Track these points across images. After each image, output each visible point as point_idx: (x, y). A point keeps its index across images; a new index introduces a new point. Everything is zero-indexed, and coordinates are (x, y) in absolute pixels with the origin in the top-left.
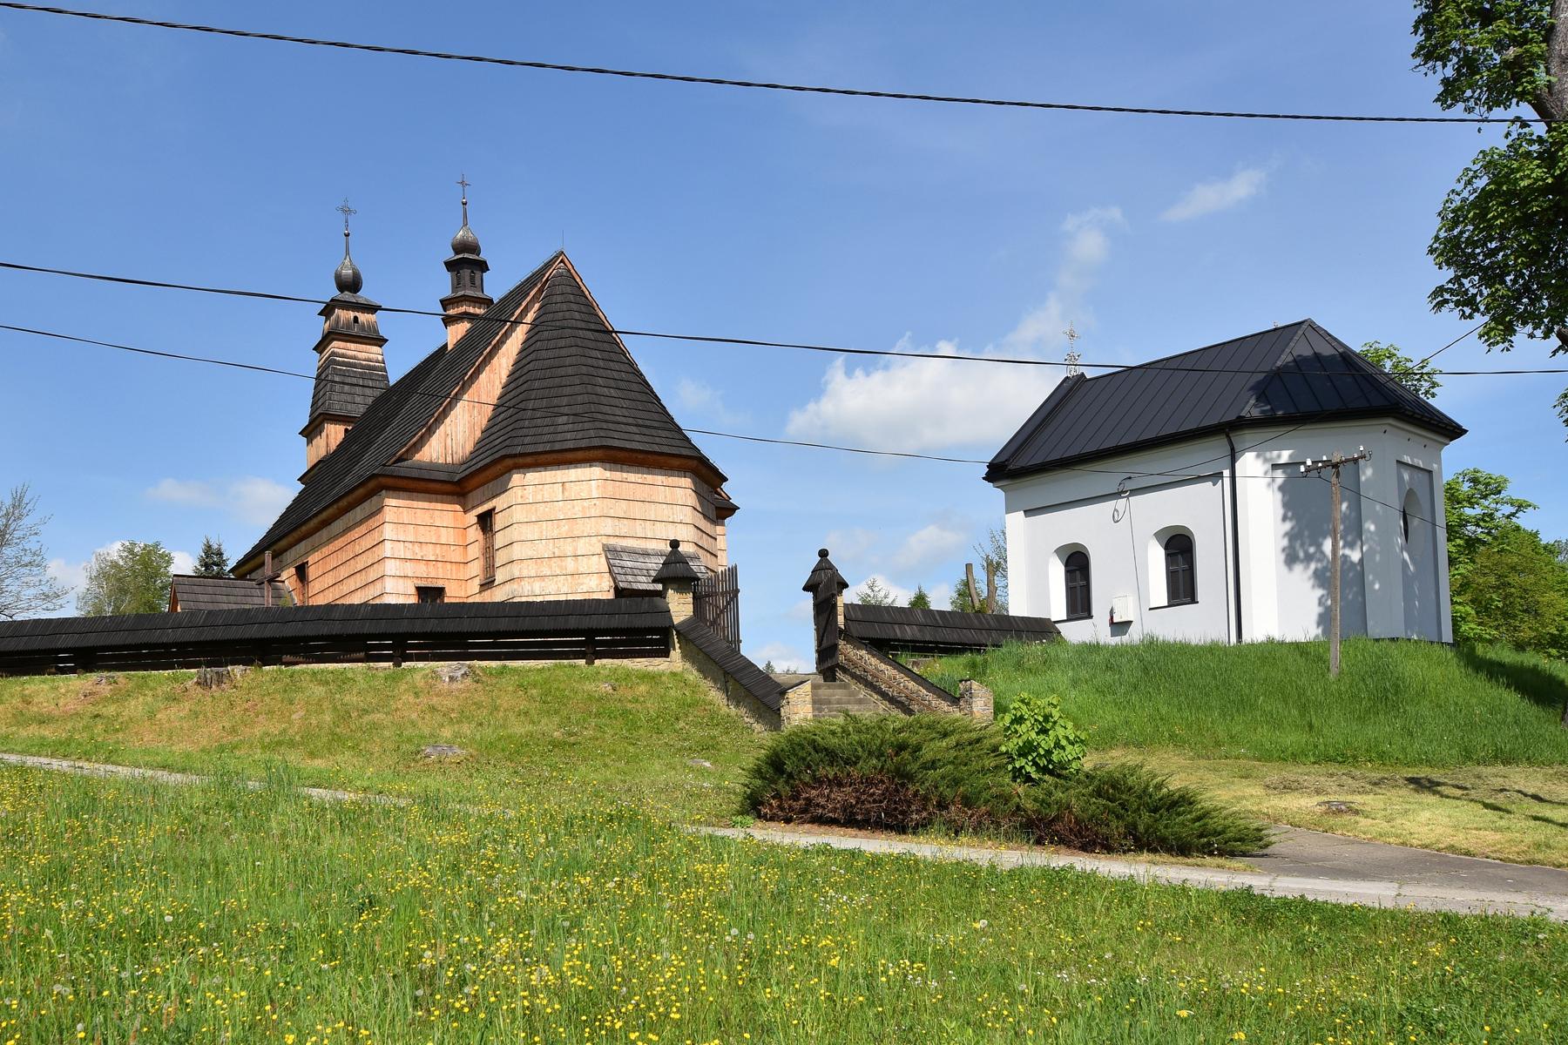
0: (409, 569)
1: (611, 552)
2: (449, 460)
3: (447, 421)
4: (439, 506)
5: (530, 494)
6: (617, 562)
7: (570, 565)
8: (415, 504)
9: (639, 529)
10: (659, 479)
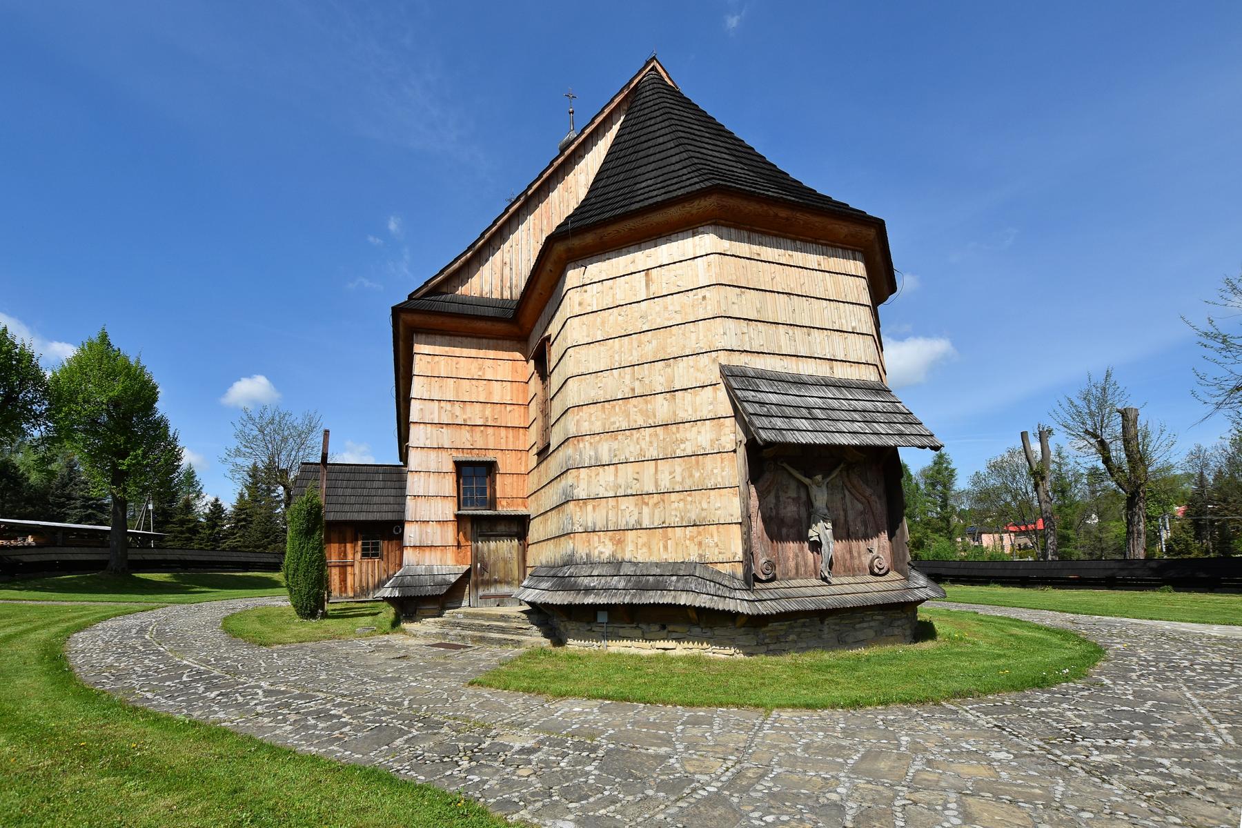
0: (446, 437)
1: (736, 381)
2: (507, 295)
3: (506, 247)
4: (492, 354)
5: (593, 298)
6: (750, 395)
7: (662, 409)
8: (457, 351)
9: (783, 340)
10: (812, 260)
